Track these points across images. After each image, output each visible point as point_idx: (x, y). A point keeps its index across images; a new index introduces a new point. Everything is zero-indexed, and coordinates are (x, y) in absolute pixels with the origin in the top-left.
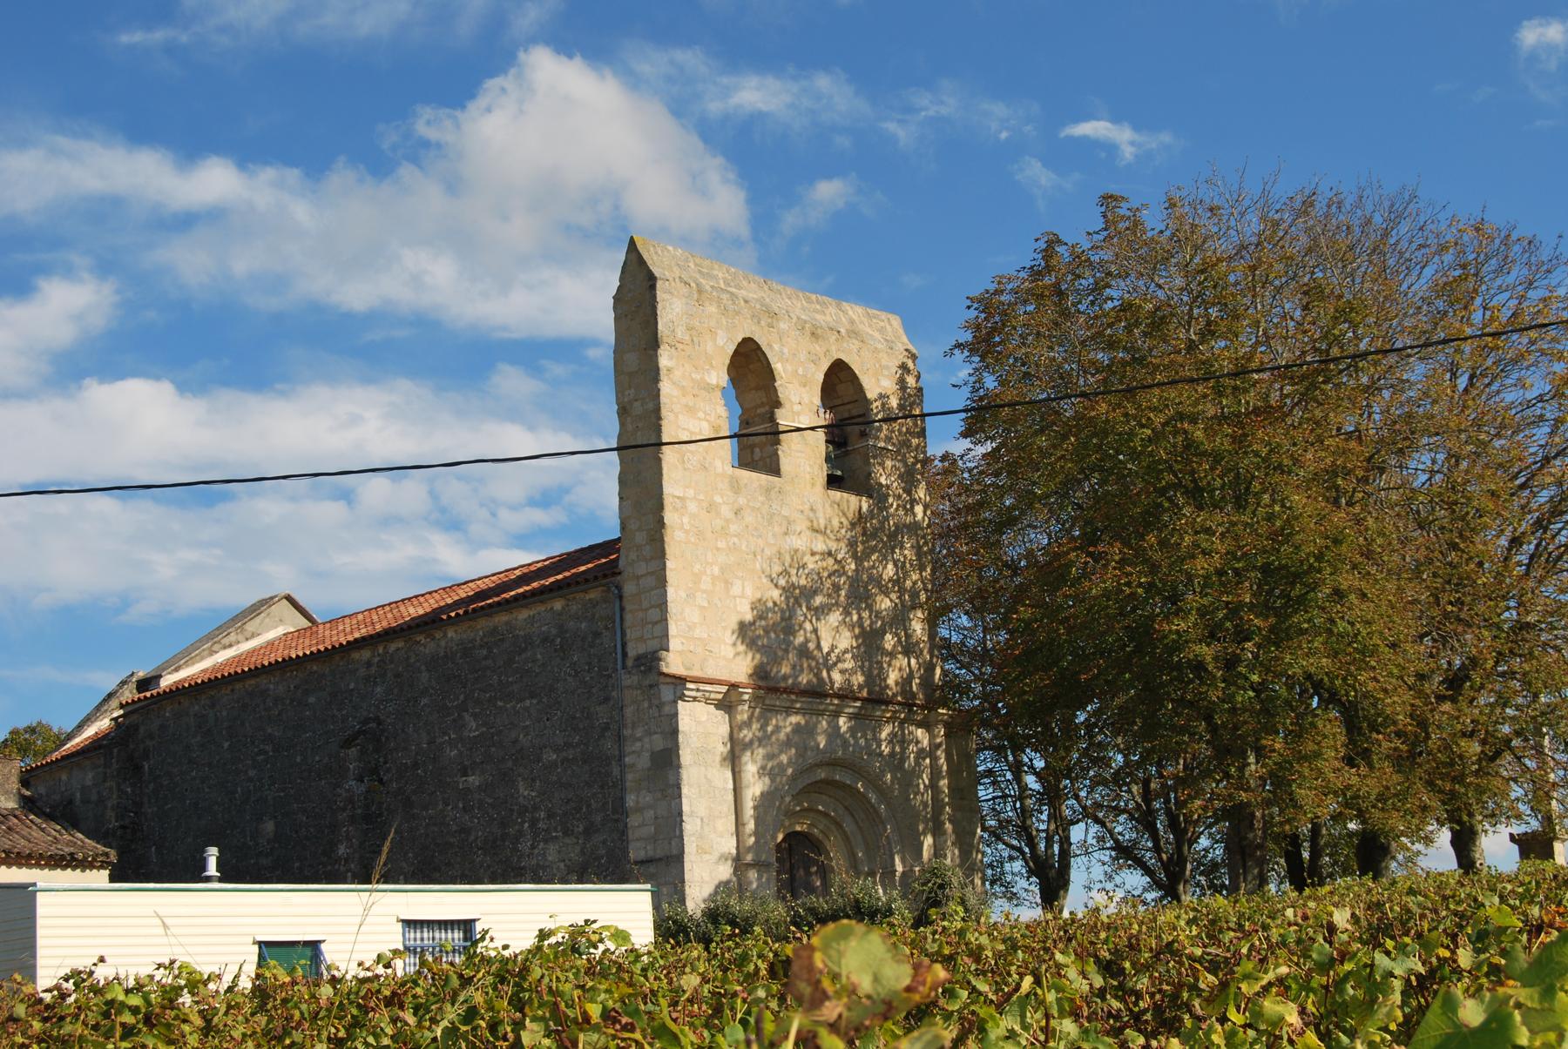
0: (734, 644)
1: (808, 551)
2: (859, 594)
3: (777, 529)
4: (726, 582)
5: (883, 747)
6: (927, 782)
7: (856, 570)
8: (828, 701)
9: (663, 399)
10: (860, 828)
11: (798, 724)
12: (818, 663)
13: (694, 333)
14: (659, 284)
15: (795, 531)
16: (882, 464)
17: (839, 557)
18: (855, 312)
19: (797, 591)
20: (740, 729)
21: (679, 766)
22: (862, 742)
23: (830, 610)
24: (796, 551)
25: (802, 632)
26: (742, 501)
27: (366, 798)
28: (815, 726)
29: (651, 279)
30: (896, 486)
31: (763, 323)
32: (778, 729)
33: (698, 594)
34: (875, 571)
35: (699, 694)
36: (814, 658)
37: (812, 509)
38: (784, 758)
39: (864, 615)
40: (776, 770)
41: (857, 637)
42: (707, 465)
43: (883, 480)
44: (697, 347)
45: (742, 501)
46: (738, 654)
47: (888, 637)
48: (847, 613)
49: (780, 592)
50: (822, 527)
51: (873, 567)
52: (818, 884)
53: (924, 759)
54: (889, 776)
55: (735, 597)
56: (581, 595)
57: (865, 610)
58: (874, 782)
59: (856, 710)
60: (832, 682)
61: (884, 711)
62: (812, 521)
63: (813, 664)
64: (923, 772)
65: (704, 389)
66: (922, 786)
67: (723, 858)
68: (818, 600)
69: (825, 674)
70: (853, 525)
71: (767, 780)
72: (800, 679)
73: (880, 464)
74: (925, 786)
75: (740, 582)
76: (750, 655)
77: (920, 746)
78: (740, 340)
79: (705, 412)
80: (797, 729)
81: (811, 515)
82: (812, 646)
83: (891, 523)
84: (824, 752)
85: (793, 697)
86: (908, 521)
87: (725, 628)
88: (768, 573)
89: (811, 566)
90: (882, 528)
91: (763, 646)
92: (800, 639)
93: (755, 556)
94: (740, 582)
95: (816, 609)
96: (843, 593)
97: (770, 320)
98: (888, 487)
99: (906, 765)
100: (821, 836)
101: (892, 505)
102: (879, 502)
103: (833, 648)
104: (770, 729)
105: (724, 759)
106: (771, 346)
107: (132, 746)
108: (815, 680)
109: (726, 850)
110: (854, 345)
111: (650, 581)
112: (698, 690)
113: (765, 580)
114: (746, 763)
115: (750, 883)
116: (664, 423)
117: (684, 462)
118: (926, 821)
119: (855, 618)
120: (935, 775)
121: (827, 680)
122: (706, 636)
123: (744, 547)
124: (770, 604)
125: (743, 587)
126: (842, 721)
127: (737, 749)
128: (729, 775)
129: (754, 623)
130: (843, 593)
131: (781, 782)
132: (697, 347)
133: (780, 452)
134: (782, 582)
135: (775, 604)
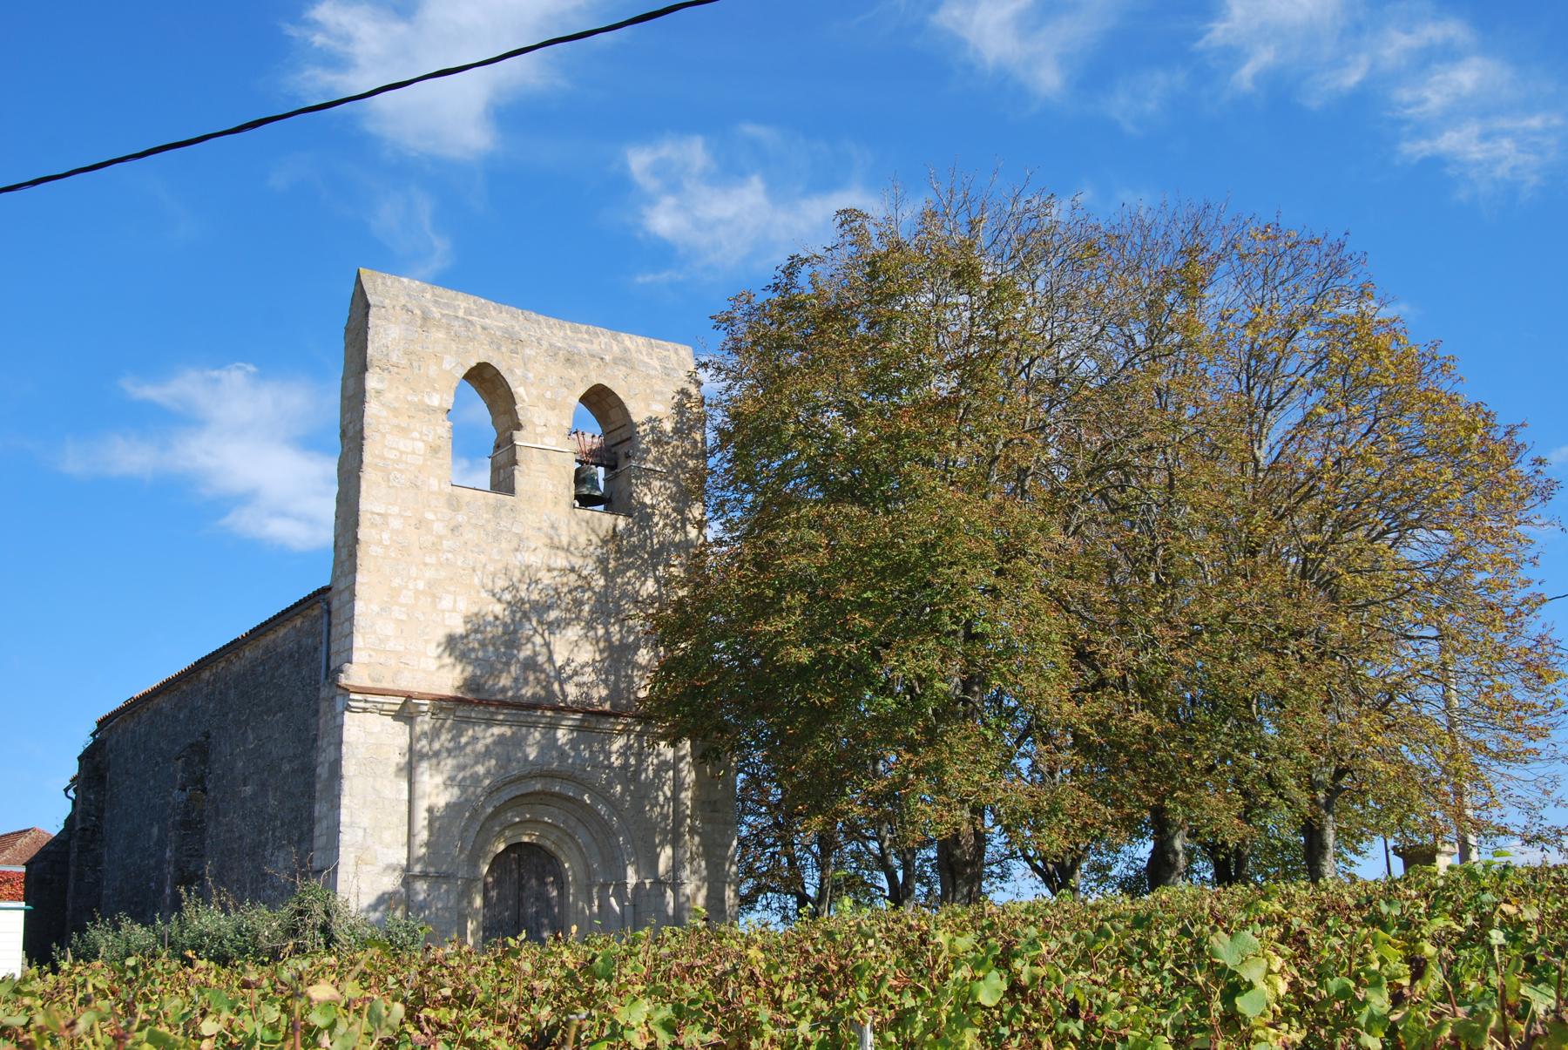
0: (439, 657)
1: (545, 567)
2: (606, 608)
3: (504, 545)
4: (434, 596)
5: (613, 759)
6: (669, 794)
7: (606, 587)
8: (539, 713)
9: (367, 420)
10: (595, 839)
11: (502, 736)
12: (548, 676)
13: (414, 357)
14: (372, 311)
15: (528, 548)
16: (648, 485)
17: (585, 573)
18: (629, 341)
19: (527, 606)
20: (419, 740)
21: (341, 777)
22: (587, 754)
23: (569, 624)
24: (528, 567)
25: (529, 646)
26: (461, 518)
27: (186, 806)
28: (525, 738)
29: (368, 306)
30: (664, 505)
31: (504, 349)
32: (475, 739)
33: (396, 608)
34: (630, 588)
35: (368, 705)
36: (543, 671)
37: (553, 527)
38: (480, 769)
39: (612, 629)
40: (468, 782)
41: (601, 652)
42: (419, 484)
43: (648, 500)
44: (416, 371)
45: (461, 518)
46: (442, 666)
47: (643, 651)
48: (590, 626)
49: (505, 606)
50: (565, 543)
51: (628, 583)
52: (555, 893)
53: (667, 771)
54: (619, 788)
55: (443, 611)
56: (309, 611)
57: (614, 624)
58: (602, 794)
59: (578, 723)
60: (565, 696)
61: (613, 724)
62: (552, 539)
63: (543, 676)
64: (664, 784)
65: (423, 410)
66: (661, 799)
67: (391, 868)
68: (553, 615)
69: (556, 687)
70: (605, 542)
71: (456, 791)
72: (523, 691)
73: (644, 485)
74: (665, 797)
75: (452, 597)
76: (459, 668)
77: (662, 758)
78: (474, 364)
79: (421, 433)
80: (501, 740)
81: (552, 532)
82: (541, 659)
83: (655, 541)
84: (533, 763)
85: (492, 709)
86: (677, 539)
87: (427, 642)
88: (490, 585)
89: (546, 582)
90: (643, 547)
91: (477, 659)
92: (526, 652)
93: (474, 570)
94: (452, 597)
95: (550, 624)
96: (586, 608)
97: (513, 347)
98: (653, 506)
99: (643, 776)
100: (553, 848)
101: (657, 524)
102: (641, 520)
103: (568, 662)
104: (463, 740)
105: (400, 770)
106: (511, 371)
107: (98, 759)
108: (543, 693)
109: (394, 861)
110: (621, 371)
111: (346, 596)
112: (366, 701)
113: (484, 595)
114: (422, 773)
115: (417, 893)
116: (365, 442)
117: (389, 480)
118: (664, 832)
119: (601, 632)
120: (678, 786)
121: (559, 694)
122: (402, 648)
123: (459, 563)
124: (491, 618)
125: (455, 602)
126: (560, 733)
127: (414, 759)
128: (405, 785)
129: (467, 636)
130: (586, 608)
131: (474, 793)
132: (416, 371)
133: (516, 472)
134: (507, 597)
135: (496, 618)
